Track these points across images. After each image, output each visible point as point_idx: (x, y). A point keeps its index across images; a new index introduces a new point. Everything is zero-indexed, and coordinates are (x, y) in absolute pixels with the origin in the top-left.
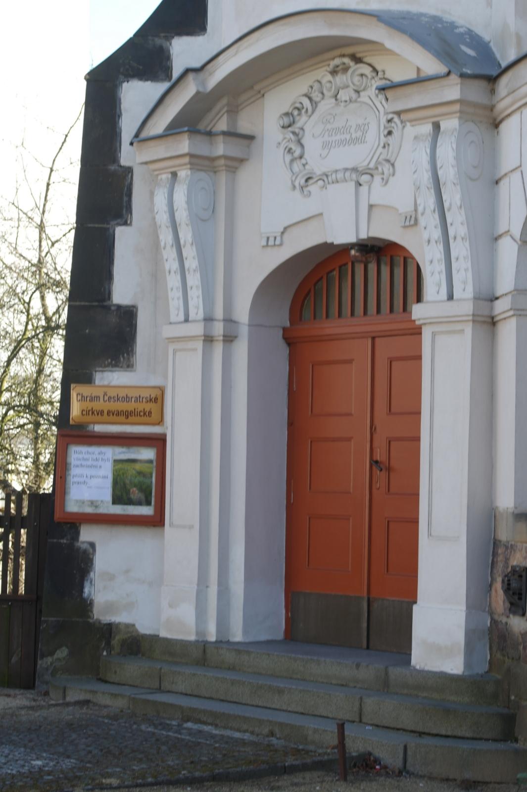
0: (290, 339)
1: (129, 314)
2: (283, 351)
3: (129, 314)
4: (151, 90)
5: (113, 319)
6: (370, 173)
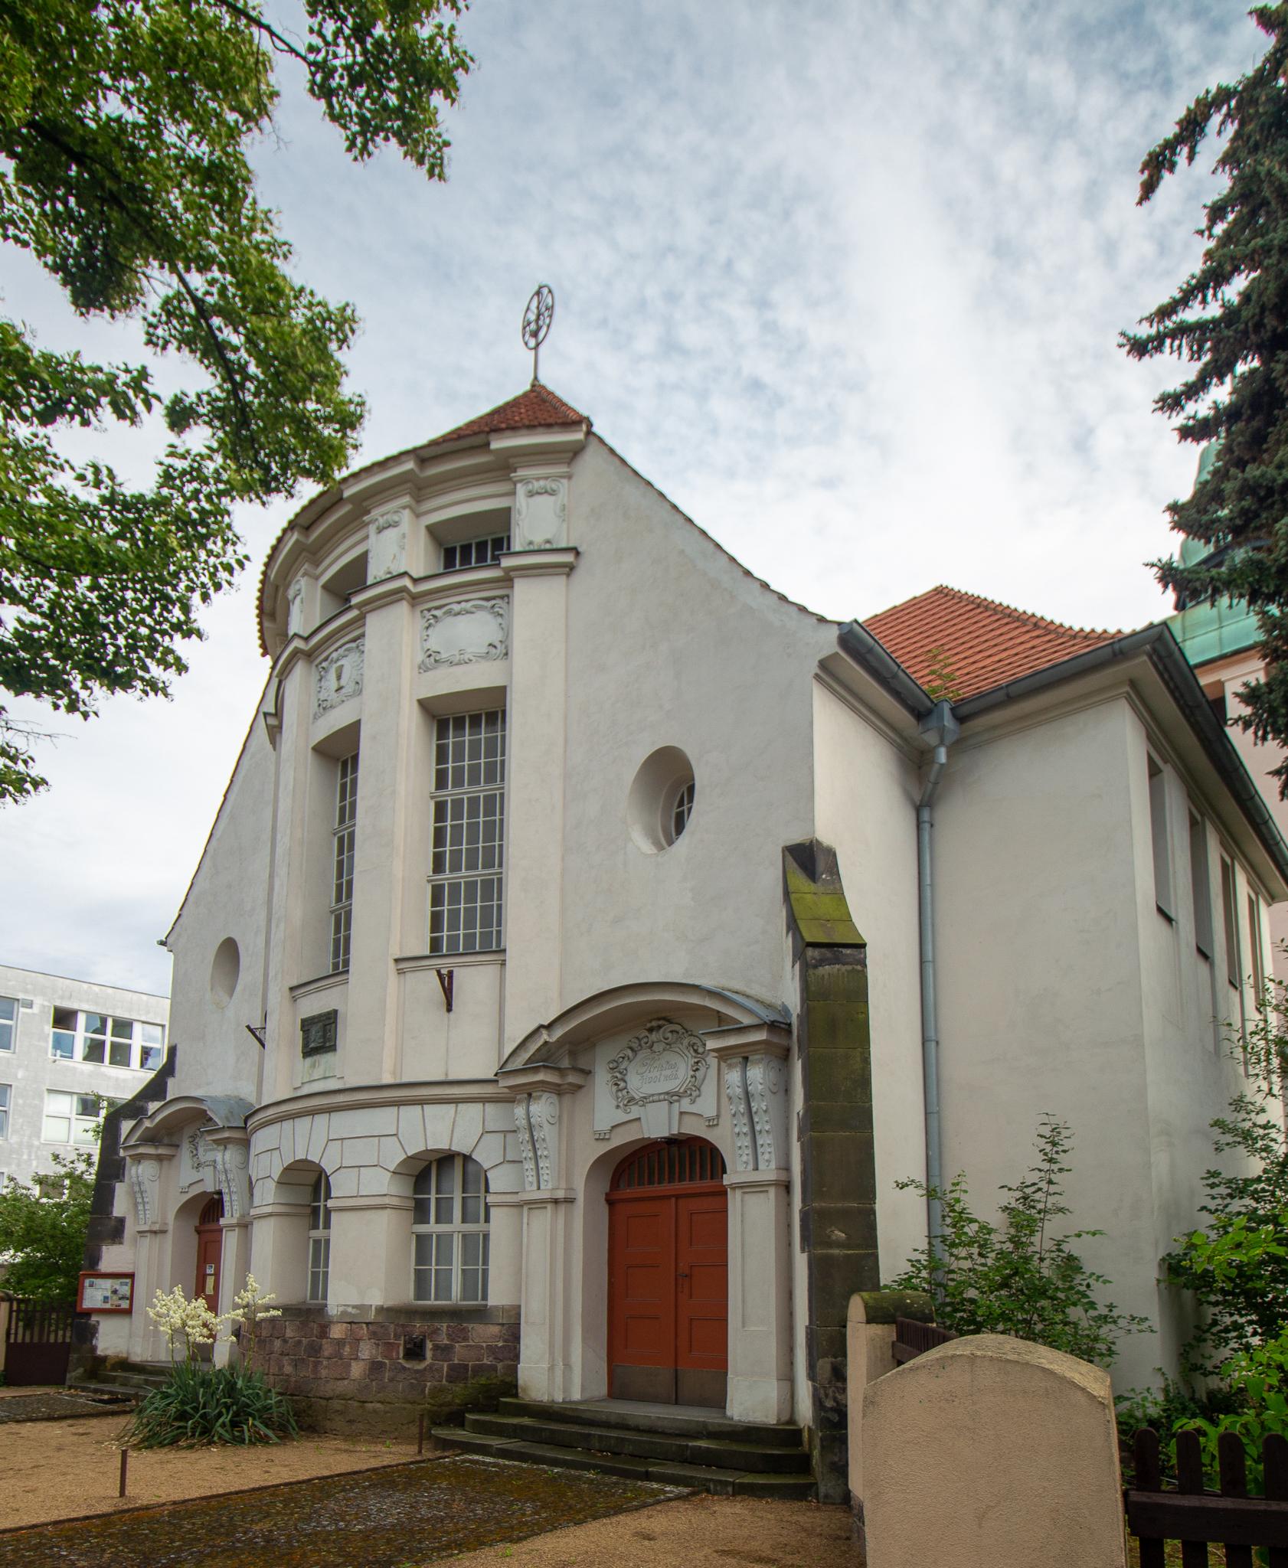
0: (198, 1232)
1: (121, 1221)
2: (196, 1236)
3: (121, 1221)
4: (132, 1123)
5: (113, 1223)
6: (676, 1094)
